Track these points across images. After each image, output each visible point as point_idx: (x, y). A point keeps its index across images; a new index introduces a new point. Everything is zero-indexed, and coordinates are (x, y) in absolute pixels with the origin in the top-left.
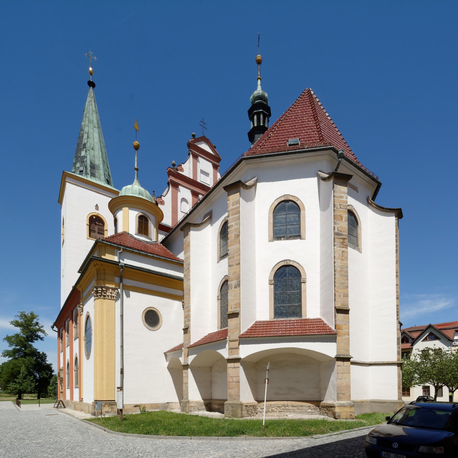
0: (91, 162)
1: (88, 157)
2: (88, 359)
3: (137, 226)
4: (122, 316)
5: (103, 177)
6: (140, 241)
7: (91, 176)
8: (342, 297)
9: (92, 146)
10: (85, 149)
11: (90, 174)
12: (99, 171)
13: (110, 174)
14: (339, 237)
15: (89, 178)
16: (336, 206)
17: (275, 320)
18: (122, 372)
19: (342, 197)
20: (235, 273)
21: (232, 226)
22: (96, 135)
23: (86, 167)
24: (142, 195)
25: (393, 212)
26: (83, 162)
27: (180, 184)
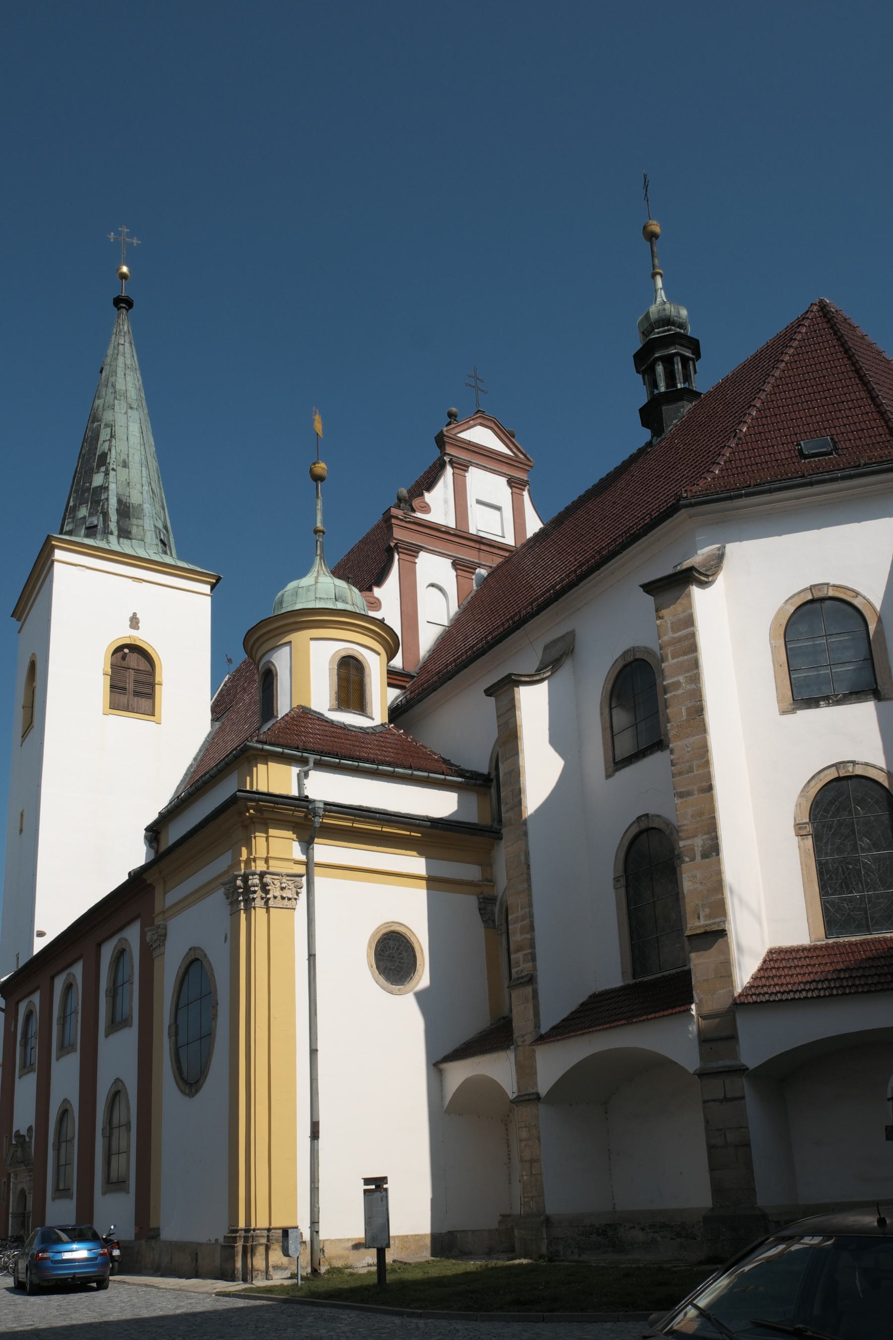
0: (120, 501)
1: (112, 487)
2: (66, 1101)
4: (312, 957)
5: (151, 537)
6: (344, 727)
7: (119, 536)
10: (103, 469)
11: (116, 533)
12: (140, 522)
15: (114, 543)
17: (830, 941)
18: (315, 1135)
20: (701, 814)
21: (677, 685)
22: (134, 428)
23: (105, 515)
24: (345, 601)
27: (421, 548)
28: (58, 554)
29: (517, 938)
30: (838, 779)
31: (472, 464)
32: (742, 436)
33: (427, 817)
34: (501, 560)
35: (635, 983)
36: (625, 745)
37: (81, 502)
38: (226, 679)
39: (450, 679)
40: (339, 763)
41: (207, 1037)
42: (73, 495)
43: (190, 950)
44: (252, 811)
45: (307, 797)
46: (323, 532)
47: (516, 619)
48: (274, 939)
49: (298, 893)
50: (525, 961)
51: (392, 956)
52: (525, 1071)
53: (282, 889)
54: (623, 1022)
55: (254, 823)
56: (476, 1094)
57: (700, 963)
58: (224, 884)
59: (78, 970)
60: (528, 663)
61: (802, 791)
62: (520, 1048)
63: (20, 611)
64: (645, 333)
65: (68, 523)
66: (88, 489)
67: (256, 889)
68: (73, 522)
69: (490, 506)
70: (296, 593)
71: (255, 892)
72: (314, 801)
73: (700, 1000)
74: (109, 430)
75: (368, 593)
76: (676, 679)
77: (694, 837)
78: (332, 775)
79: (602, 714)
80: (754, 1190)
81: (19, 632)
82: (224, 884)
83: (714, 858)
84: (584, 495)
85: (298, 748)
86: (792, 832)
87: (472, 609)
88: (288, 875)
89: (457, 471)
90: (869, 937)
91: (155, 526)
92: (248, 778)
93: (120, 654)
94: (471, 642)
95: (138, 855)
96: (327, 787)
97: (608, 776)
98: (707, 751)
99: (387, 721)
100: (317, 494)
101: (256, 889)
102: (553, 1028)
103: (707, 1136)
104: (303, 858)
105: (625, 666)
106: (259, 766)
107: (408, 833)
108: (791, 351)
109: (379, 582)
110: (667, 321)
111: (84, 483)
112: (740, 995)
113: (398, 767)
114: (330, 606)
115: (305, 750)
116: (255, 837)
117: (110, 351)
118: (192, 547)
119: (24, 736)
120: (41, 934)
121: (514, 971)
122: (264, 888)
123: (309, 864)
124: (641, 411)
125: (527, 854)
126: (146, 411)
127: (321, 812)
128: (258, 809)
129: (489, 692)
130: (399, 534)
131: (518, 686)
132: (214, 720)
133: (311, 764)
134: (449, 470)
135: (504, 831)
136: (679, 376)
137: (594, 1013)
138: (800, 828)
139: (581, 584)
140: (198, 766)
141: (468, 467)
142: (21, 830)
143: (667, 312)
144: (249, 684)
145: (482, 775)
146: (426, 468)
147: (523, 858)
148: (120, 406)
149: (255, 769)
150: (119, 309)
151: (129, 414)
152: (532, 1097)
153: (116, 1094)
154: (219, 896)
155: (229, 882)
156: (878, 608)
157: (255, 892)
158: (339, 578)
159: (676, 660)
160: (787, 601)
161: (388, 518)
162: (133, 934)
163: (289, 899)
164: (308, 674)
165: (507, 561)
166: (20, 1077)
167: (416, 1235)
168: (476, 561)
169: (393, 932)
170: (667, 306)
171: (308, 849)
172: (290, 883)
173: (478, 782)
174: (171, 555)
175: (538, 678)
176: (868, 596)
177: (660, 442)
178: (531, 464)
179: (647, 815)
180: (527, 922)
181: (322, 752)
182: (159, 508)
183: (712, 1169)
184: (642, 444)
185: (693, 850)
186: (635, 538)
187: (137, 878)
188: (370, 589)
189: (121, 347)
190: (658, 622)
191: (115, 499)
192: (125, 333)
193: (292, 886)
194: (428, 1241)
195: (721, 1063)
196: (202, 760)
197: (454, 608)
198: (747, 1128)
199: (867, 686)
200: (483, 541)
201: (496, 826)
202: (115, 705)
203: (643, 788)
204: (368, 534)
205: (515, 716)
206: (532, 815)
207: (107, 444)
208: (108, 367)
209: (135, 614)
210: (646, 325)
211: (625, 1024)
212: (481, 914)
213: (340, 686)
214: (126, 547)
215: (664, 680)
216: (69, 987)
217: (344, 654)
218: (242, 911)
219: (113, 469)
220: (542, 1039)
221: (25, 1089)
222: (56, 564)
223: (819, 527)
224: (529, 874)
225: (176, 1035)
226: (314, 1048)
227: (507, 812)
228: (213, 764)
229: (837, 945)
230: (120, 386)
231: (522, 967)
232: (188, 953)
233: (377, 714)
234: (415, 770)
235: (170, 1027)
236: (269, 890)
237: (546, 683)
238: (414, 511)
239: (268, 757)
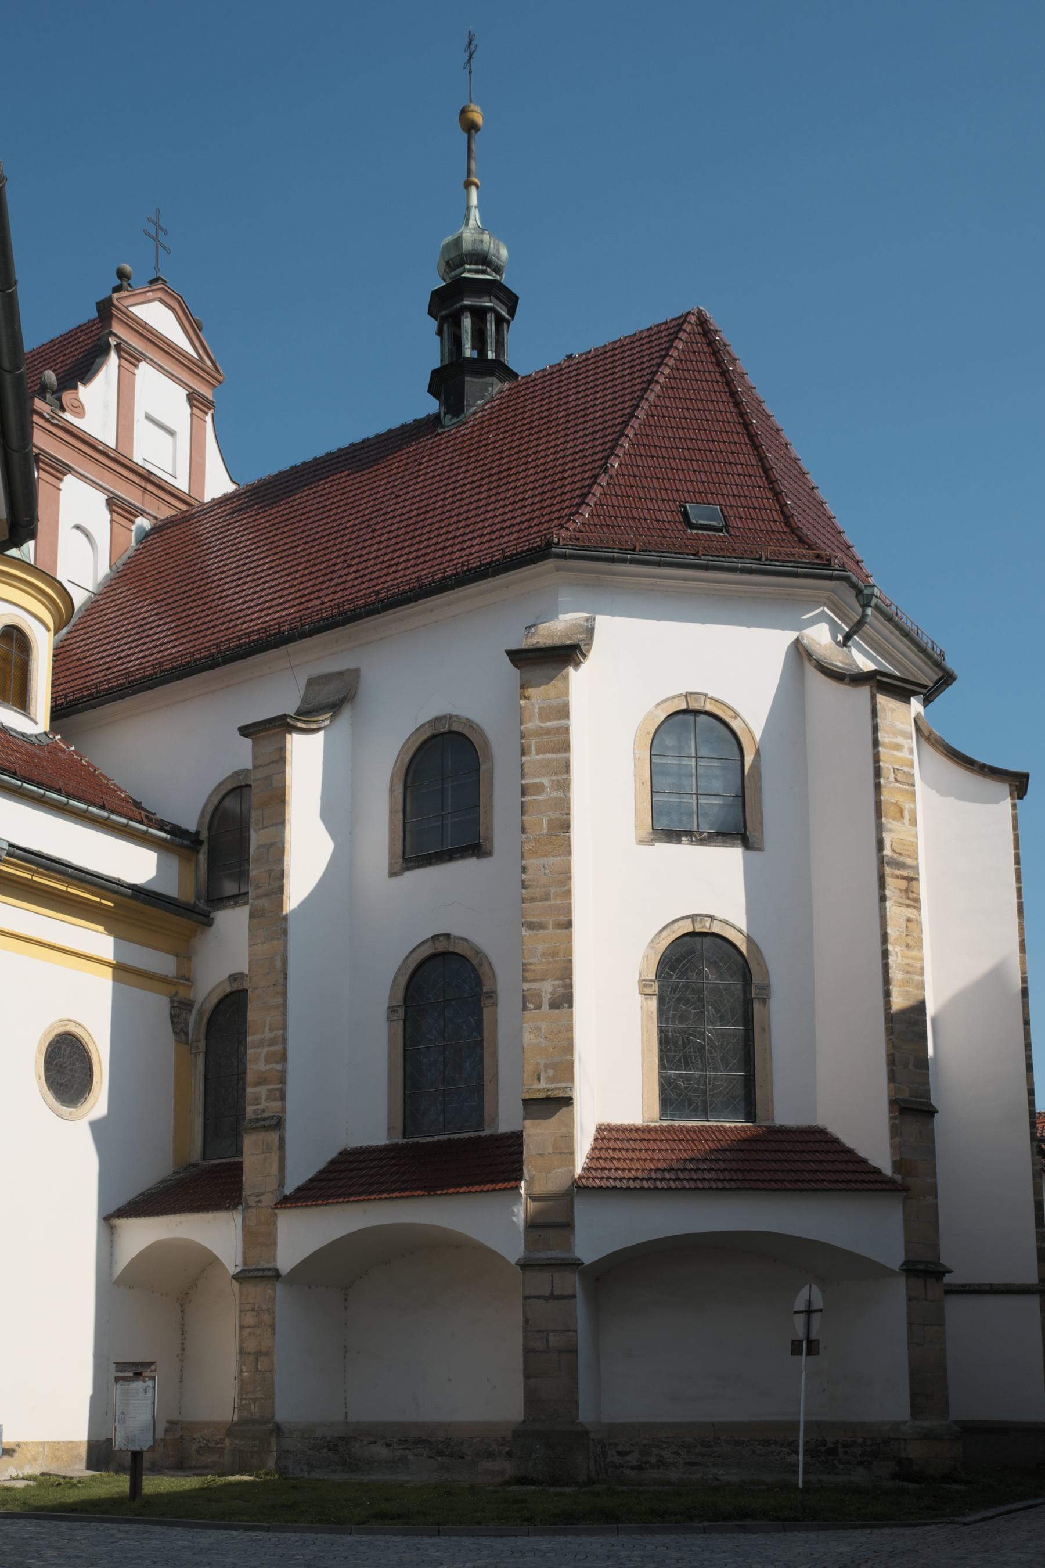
8: (911, 1067)
14: (898, 872)
16: (884, 772)
17: (665, 1124)
19: (898, 747)
20: (554, 954)
25: (1003, 781)
27: (68, 469)
30: (692, 934)
31: (145, 358)
32: (614, 473)
35: (407, 1143)
40: (21, 787)
50: (268, 1099)
51: (66, 1066)
57: (537, 1135)
61: (652, 941)
73: (532, 1178)
76: (538, 780)
77: (543, 980)
79: (392, 791)
80: (577, 1402)
83: (564, 1011)
86: (635, 987)
89: (124, 363)
90: (707, 1124)
97: (393, 874)
98: (570, 878)
99: (48, 729)
102: (299, 1189)
103: (525, 1338)
105: (433, 737)
107: (98, 899)
108: (667, 371)
110: (482, 259)
112: (580, 1177)
125: (285, 960)
129: (245, 731)
131: (290, 733)
134: (113, 359)
136: (491, 341)
137: (347, 1177)
138: (645, 986)
143: (485, 247)
147: (278, 964)
152: (270, 1273)
156: (758, 737)
159: (541, 756)
160: (658, 704)
167: (69, 1442)
168: (138, 505)
169: (68, 1034)
176: (748, 721)
178: (221, 378)
183: (527, 1376)
184: (421, 415)
185: (540, 996)
190: (522, 702)
194: (83, 1451)
195: (551, 1254)
198: (575, 1331)
199: (737, 829)
200: (152, 478)
203: (447, 900)
205: (284, 772)
206: (294, 910)
212: (173, 1023)
223: (704, 622)
224: (285, 986)
229: (670, 1129)
237: (322, 733)
238: (63, 409)
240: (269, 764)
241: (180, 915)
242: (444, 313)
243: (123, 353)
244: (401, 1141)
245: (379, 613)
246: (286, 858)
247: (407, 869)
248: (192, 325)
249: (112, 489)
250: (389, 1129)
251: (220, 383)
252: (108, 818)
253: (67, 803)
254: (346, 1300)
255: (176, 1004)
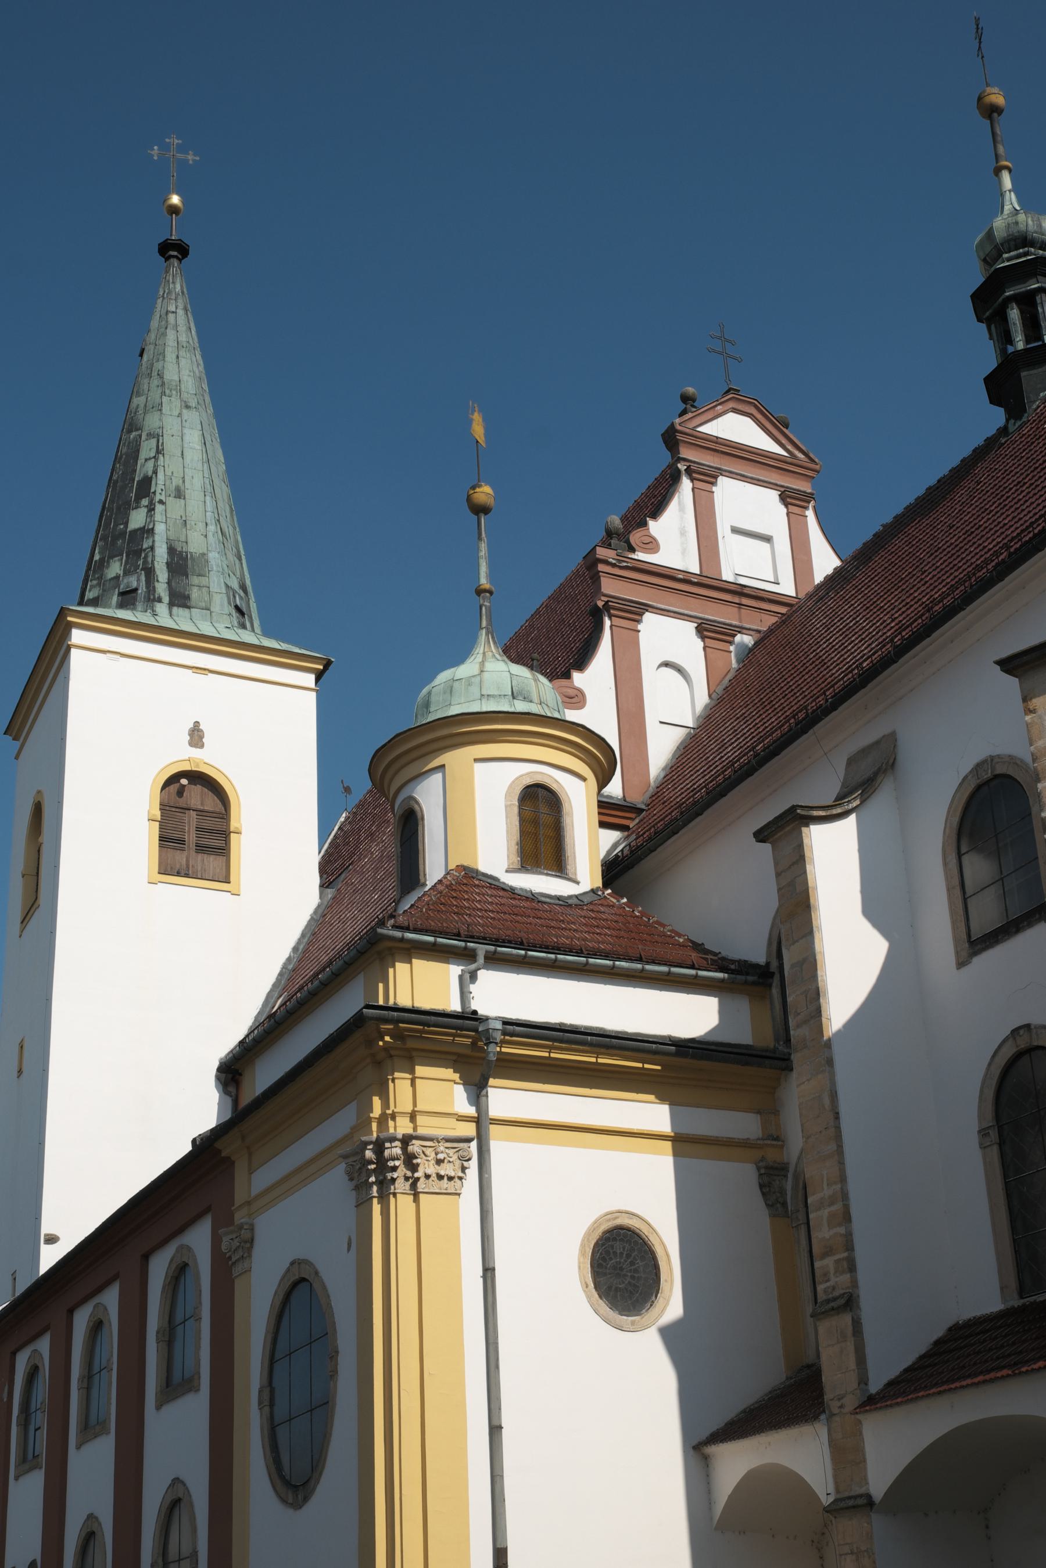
0: (171, 550)
1: (160, 528)
2: (91, 1517)
3: (516, 836)
4: (488, 1272)
5: (220, 603)
6: (532, 898)
7: (171, 604)
9: (176, 481)
10: (145, 502)
12: (203, 581)
13: (248, 582)
15: (163, 616)
22: (193, 438)
23: (150, 573)
24: (527, 699)
26: (137, 553)
27: (646, 608)
28: (77, 636)
29: (823, 1234)
31: (721, 472)
33: (670, 1037)
34: (774, 620)
35: (1024, 1305)
36: (987, 913)
37: (111, 553)
38: (342, 819)
39: (699, 814)
40: (525, 956)
41: (321, 1408)
42: (100, 543)
43: (292, 1263)
44: (387, 1038)
45: (475, 1012)
46: (491, 593)
47: (801, 716)
48: (426, 1240)
49: (463, 1169)
51: (620, 1267)
52: (847, 1457)
53: (439, 1162)
54: (1005, 1372)
55: (391, 1056)
56: (766, 1488)
58: (345, 1157)
59: (111, 1298)
60: (823, 785)
62: (837, 1419)
63: (19, 725)
64: (987, 261)
65: (92, 587)
66: (123, 533)
67: (397, 1163)
68: (99, 584)
69: (756, 535)
70: (450, 689)
71: (394, 1169)
72: (486, 1019)
74: (154, 442)
75: (563, 682)
78: (514, 975)
79: (945, 864)
81: (17, 758)
82: (345, 1157)
84: (903, 515)
85: (458, 935)
87: (729, 700)
88: (447, 1140)
89: (699, 484)
91: (227, 586)
92: (381, 985)
93: (174, 788)
94: (731, 753)
95: (203, 1110)
96: (507, 995)
97: (961, 964)
100: (480, 534)
101: (397, 1163)
102: (891, 1384)
104: (472, 1111)
105: (979, 788)
106: (398, 964)
107: (640, 1065)
109: (581, 661)
110: (1023, 240)
111: (116, 525)
113: (619, 959)
114: (505, 707)
115: (471, 938)
116: (393, 1080)
117: (154, 324)
118: (284, 611)
119: (25, 920)
120: (51, 1240)
121: (820, 1288)
122: (410, 1161)
123: (481, 1121)
124: (988, 380)
125: (834, 1096)
126: (210, 410)
127: (499, 1037)
128: (397, 1035)
129: (761, 836)
130: (610, 587)
131: (807, 825)
132: (324, 885)
133: (481, 960)
134: (686, 484)
135: (795, 1058)
137: (957, 1357)
139: (901, 661)
140: (300, 961)
141: (716, 477)
142: (20, 1072)
143: (1022, 227)
144: (379, 826)
145: (756, 966)
146: (650, 481)
147: (827, 1101)
148: (171, 406)
149: (391, 970)
150: (167, 259)
151: (185, 417)
152: (860, 1502)
153: (175, 1504)
154: (337, 1175)
155: (355, 1154)
157: (394, 1169)
158: (517, 663)
161: (591, 563)
162: (199, 1239)
163: (450, 1179)
164: (472, 817)
165: (783, 622)
166: (17, 1478)
169: (620, 1228)
170: (1021, 217)
171: (478, 1096)
172: (451, 1152)
173: (750, 978)
174: (253, 630)
175: (839, 810)
177: (1021, 427)
178: (817, 467)
179: (1028, 1026)
180: (838, 1207)
181: (497, 940)
182: (232, 558)
184: (991, 431)
186: (985, 586)
187: (206, 1148)
188: (567, 676)
189: (171, 317)
190: (1028, 718)
191: (165, 546)
192: (177, 295)
193: (454, 1158)
196: (306, 951)
197: (702, 699)
200: (746, 591)
201: (782, 1048)
202: (167, 869)
204: (562, 587)
205: (805, 872)
206: (839, 1032)
207: (150, 465)
208: (152, 347)
209: (197, 724)
210: (988, 248)
211: (1008, 1376)
212: (763, 1194)
213: (523, 833)
214: (182, 620)
215: (1042, 810)
216: (97, 1327)
217: (529, 781)
218: (375, 1201)
219: (161, 502)
220: (871, 1402)
221: (26, 1494)
222: (73, 651)
224: (838, 1128)
225: (272, 1404)
226: (495, 1423)
227: (798, 1026)
228: (325, 959)
230: (171, 374)
231: (836, 1282)
232: (288, 1270)
233: (585, 874)
234: (648, 963)
235: (260, 1392)
236: (418, 1165)
237: (853, 817)
238: (632, 550)
239: (411, 951)
240: (790, 867)
241: (747, 1064)
242: (988, 314)
243: (694, 475)
244: (1017, 1303)
245: (895, 662)
246: (819, 973)
247: (975, 953)
248: (774, 423)
249: (701, 615)
250: (1002, 1289)
251: (818, 472)
252: (643, 970)
253: (587, 963)
254: (987, 1527)
255: (763, 1171)
